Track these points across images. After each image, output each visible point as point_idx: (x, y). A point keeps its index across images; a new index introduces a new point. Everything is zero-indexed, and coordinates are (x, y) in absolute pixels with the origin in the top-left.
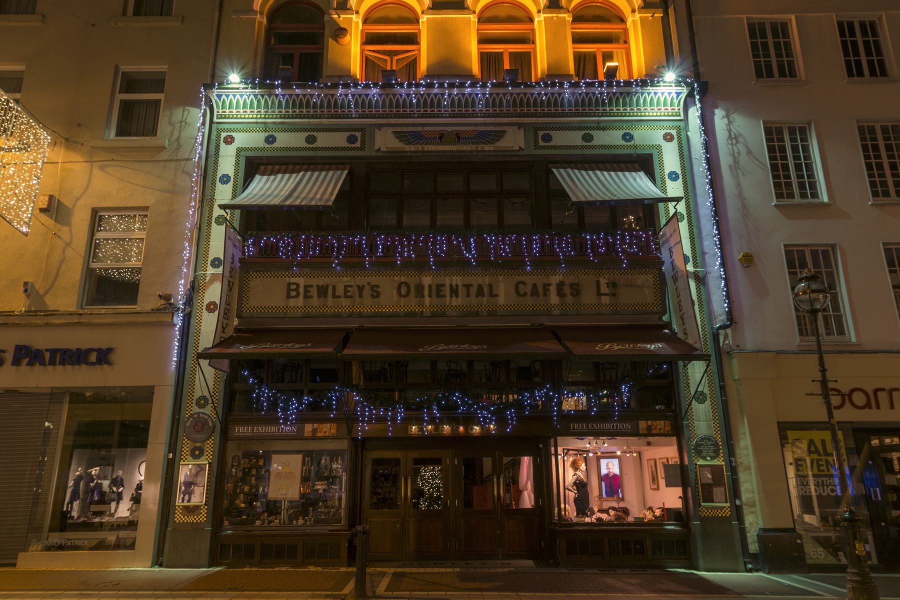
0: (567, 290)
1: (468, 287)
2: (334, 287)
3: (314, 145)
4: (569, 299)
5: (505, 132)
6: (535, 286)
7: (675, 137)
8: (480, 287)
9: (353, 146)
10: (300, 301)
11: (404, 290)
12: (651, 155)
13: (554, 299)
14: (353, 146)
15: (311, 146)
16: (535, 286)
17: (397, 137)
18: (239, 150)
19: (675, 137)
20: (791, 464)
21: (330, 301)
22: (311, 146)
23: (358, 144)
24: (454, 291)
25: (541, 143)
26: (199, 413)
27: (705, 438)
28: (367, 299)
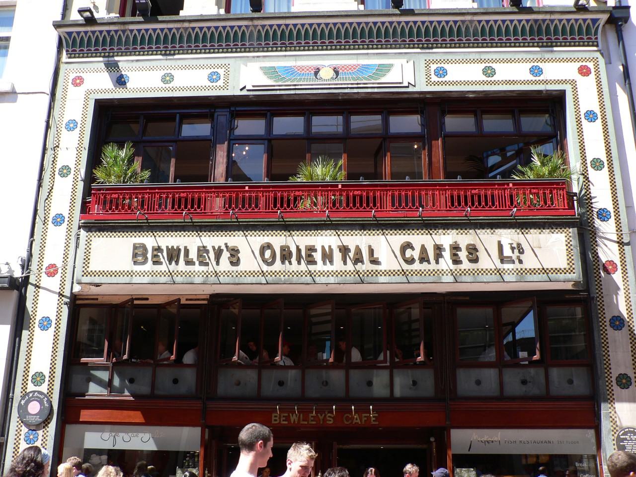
0: (463, 255)
1: (344, 250)
2: (187, 252)
3: (583, 120)
4: (466, 265)
5: (391, 65)
6: (423, 249)
7: (593, 70)
8: (358, 251)
9: (537, 78)
10: (149, 266)
11: (268, 254)
12: (563, 93)
13: (446, 262)
14: (537, 78)
15: (582, 116)
16: (423, 249)
17: (265, 73)
18: (88, 93)
19: (593, 70)
20: (167, 79)
21: (182, 266)
22: (582, 116)
23: (434, 67)
24: (328, 256)
25: (434, 78)
26: (34, 392)
27: (631, 432)
28: (225, 264)
